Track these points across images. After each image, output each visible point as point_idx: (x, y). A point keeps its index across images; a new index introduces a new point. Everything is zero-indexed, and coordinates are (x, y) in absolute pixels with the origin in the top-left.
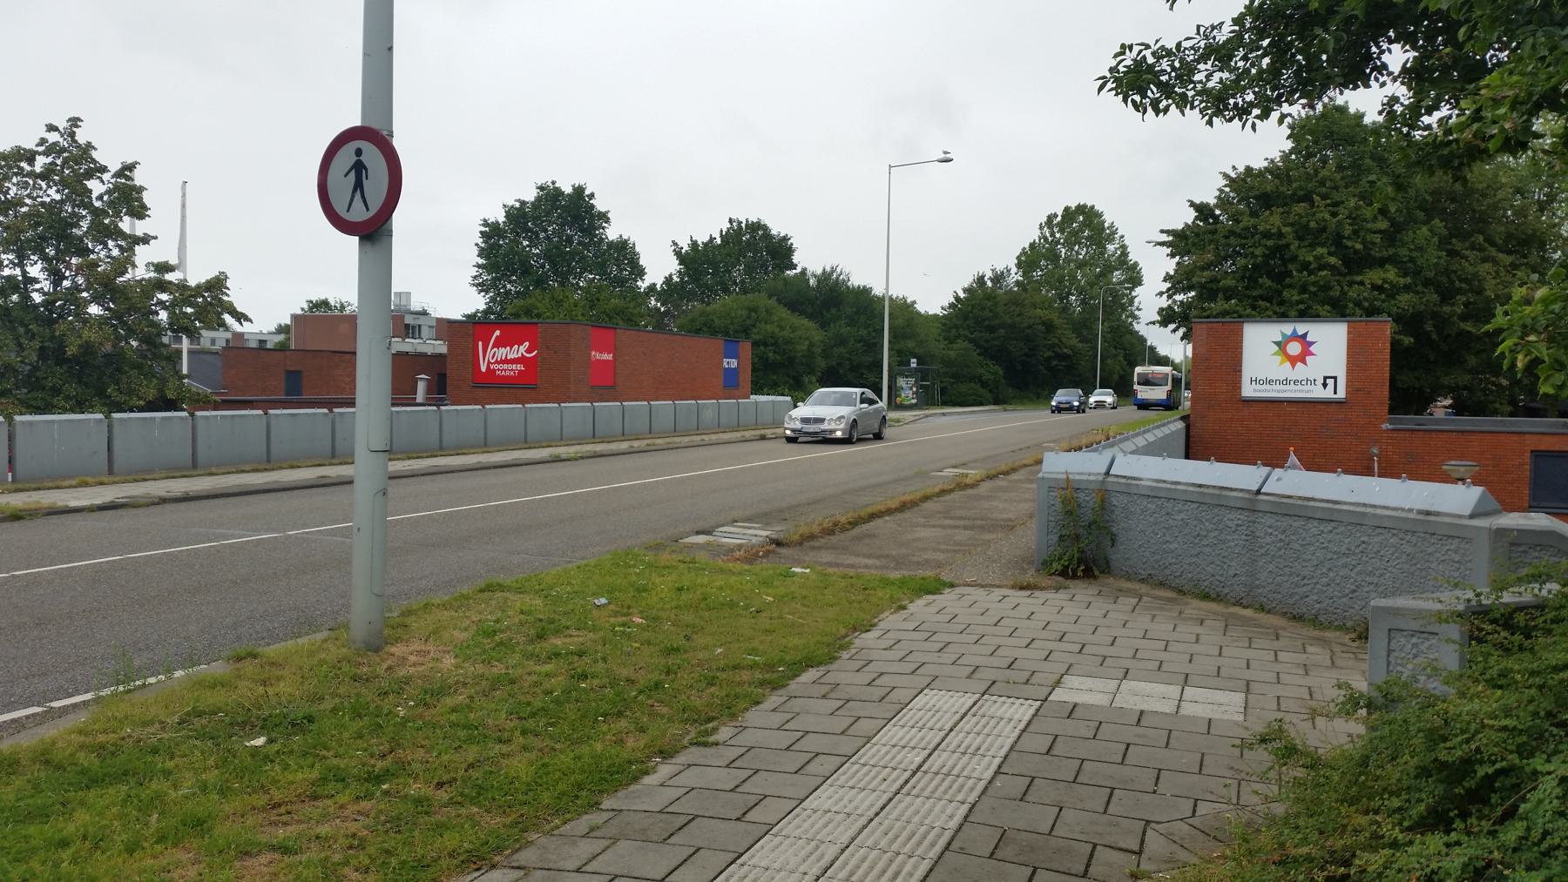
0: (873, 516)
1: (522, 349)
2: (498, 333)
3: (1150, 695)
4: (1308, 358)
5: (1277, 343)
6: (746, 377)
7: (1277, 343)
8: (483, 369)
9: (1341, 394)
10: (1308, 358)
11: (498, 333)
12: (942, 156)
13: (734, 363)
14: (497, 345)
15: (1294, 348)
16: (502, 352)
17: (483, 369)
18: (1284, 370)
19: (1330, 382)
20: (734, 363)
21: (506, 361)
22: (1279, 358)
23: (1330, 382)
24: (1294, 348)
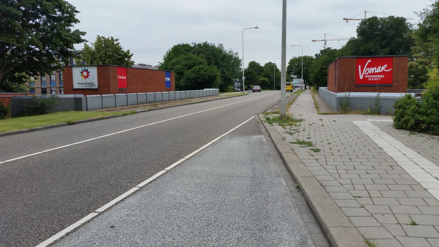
0: (326, 114)
1: (383, 68)
2: (370, 61)
3: (379, 120)
4: (89, 77)
5: (81, 72)
6: (173, 86)
7: (81, 72)
8: (361, 78)
10: (89, 77)
11: (370, 61)
12: (256, 27)
13: (169, 79)
14: (369, 66)
15: (85, 74)
16: (372, 70)
17: (361, 78)
20: (169, 79)
21: (374, 74)
22: (82, 77)
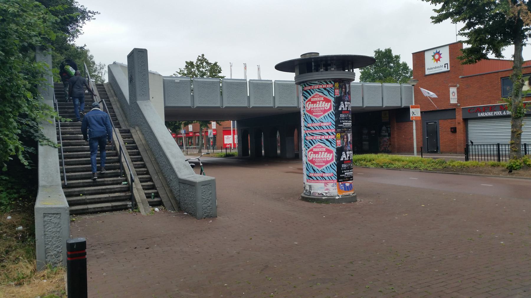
9: (449, 69)
15: (437, 57)
18: (435, 64)
19: (446, 65)
23: (446, 65)
24: (437, 57)
